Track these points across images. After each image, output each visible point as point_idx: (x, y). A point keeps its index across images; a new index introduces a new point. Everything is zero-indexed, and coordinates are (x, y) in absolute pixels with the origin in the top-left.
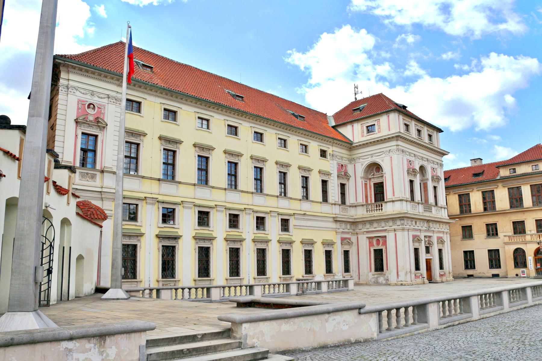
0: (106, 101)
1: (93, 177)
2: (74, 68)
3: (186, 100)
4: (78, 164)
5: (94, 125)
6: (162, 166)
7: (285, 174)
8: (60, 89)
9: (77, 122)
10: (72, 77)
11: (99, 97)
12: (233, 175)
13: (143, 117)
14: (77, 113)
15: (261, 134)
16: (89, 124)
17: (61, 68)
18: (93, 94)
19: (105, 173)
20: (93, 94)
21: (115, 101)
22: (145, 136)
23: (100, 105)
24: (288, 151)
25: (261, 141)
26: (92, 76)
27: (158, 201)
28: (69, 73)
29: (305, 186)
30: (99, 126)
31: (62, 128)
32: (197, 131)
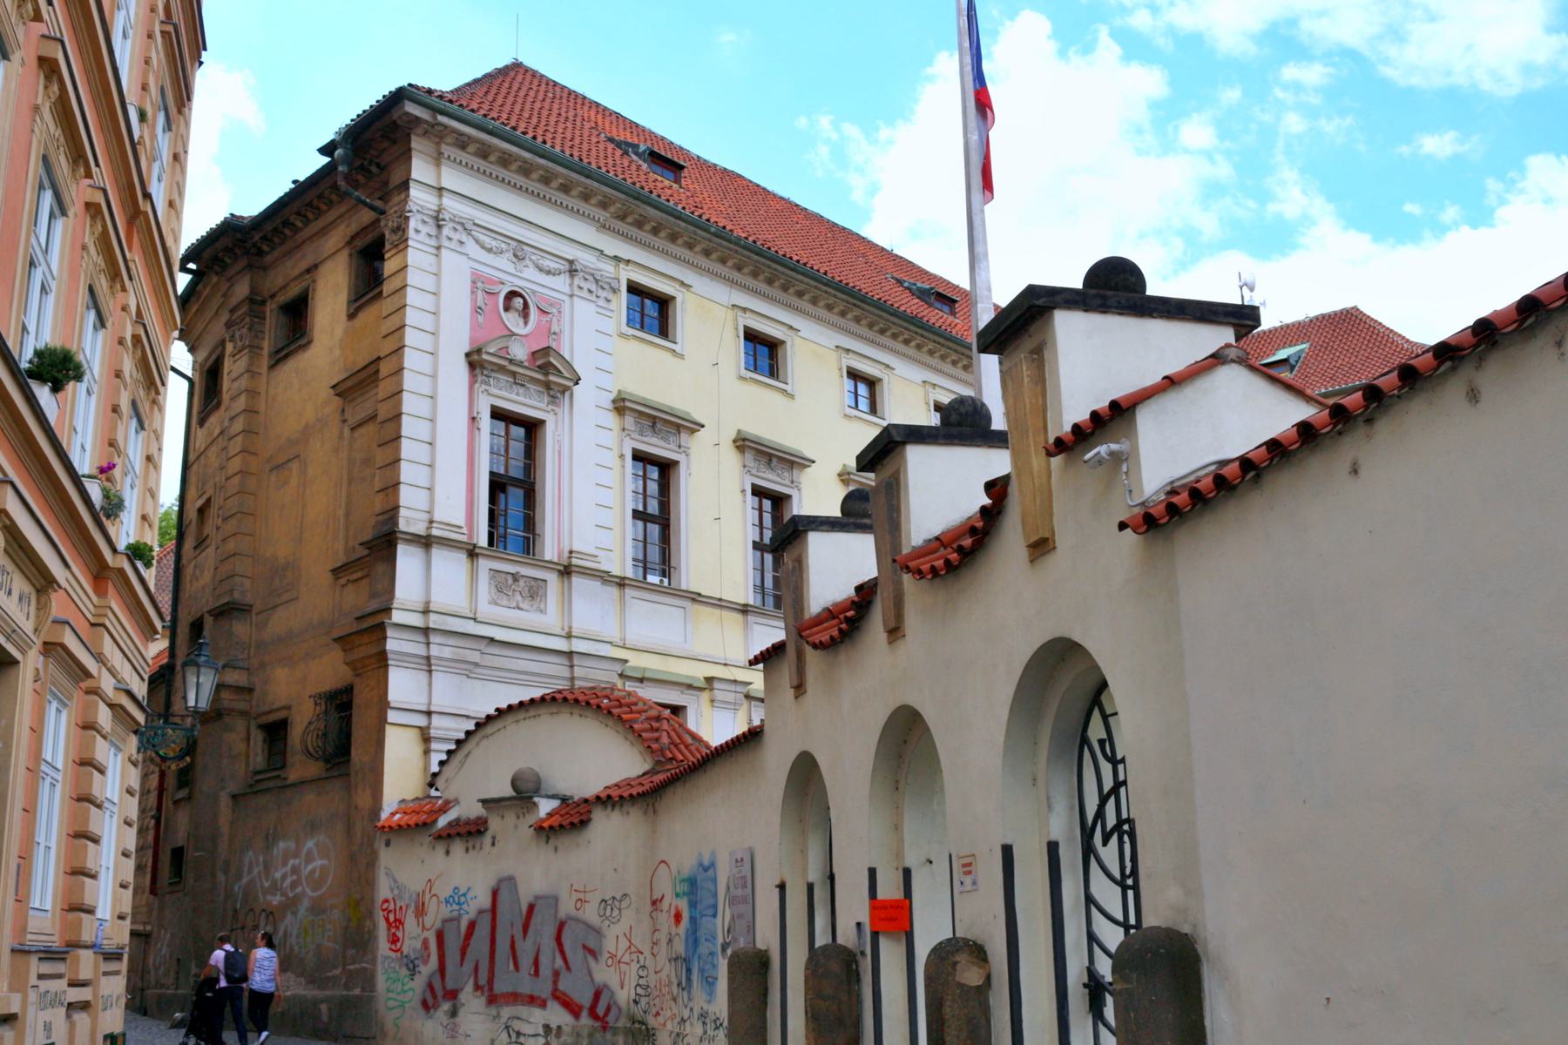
0: (561, 283)
1: (535, 591)
2: (462, 143)
3: (814, 301)
4: (483, 541)
5: (533, 380)
6: (632, 529)
7: (666, 468)
8: (412, 224)
9: (475, 362)
10: (451, 178)
11: (541, 270)
12: (516, 482)
13: (681, 356)
14: (473, 329)
15: (664, 303)
16: (514, 374)
17: (416, 143)
18: (520, 251)
19: (575, 579)
20: (520, 251)
21: (593, 288)
22: (693, 431)
23: (546, 301)
24: (681, 356)
25: (773, 372)
26: (520, 180)
27: (748, 697)
28: (438, 164)
29: (653, 507)
30: (548, 386)
31: (424, 386)
32: (846, 422)
